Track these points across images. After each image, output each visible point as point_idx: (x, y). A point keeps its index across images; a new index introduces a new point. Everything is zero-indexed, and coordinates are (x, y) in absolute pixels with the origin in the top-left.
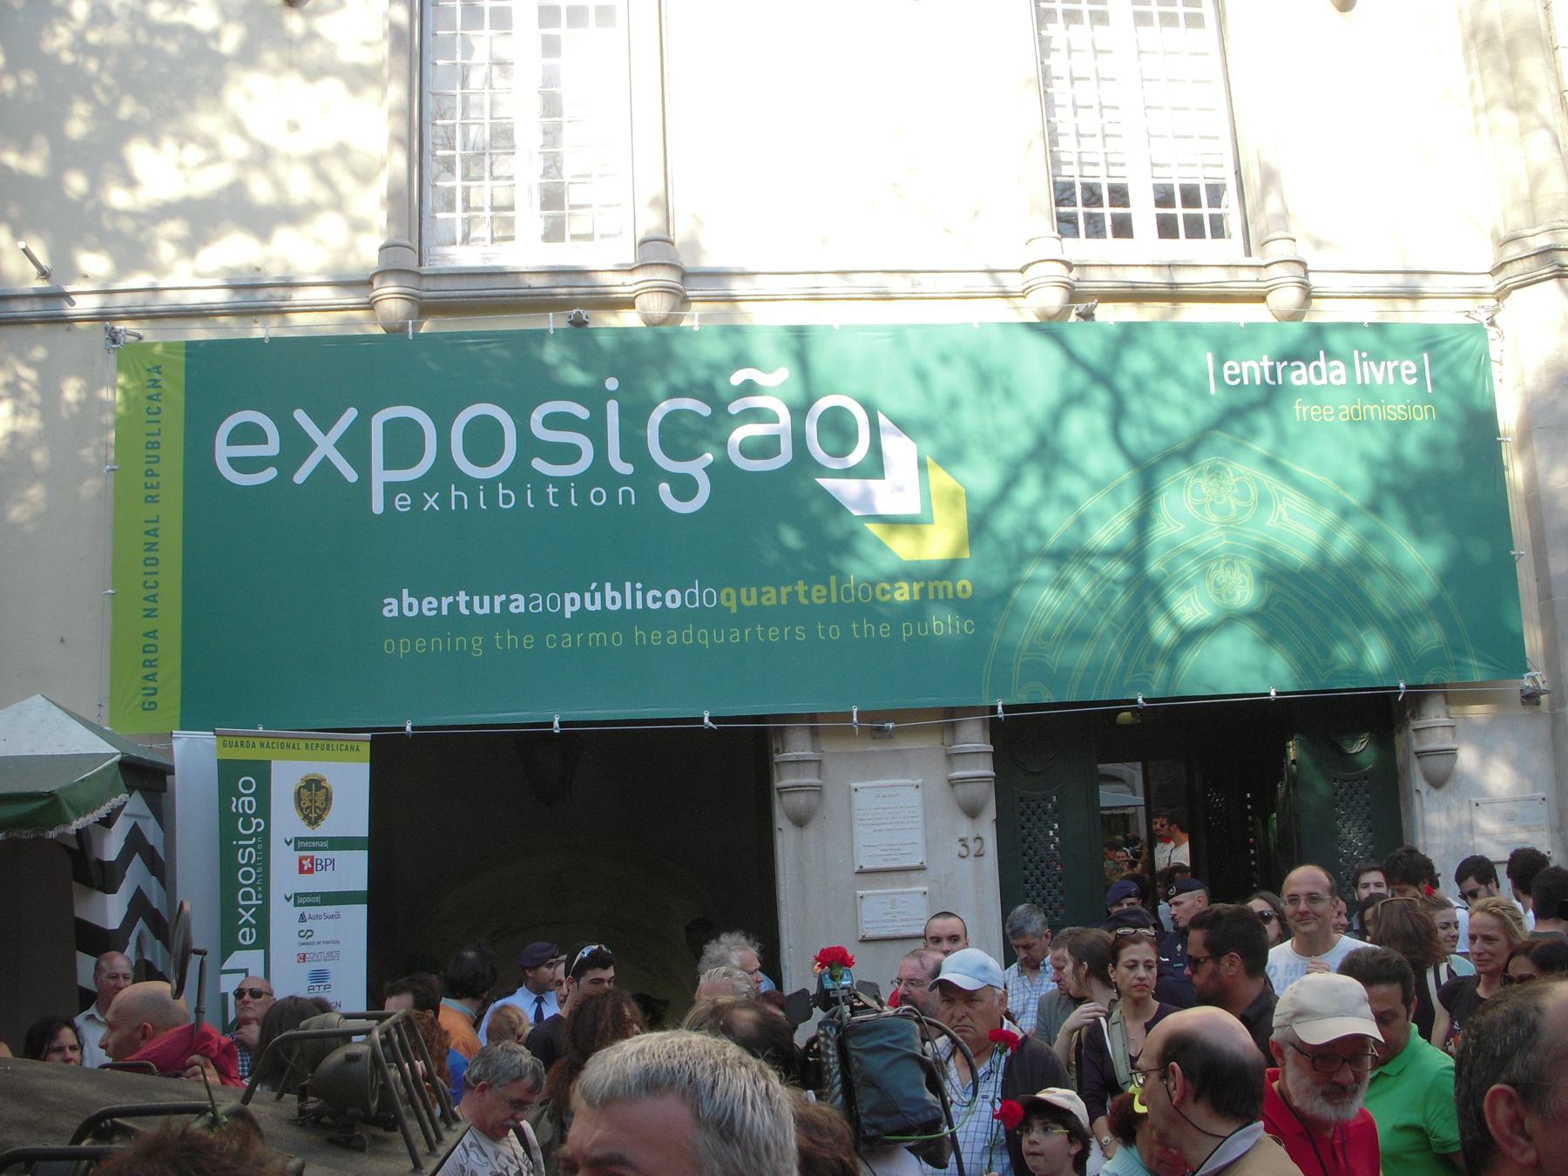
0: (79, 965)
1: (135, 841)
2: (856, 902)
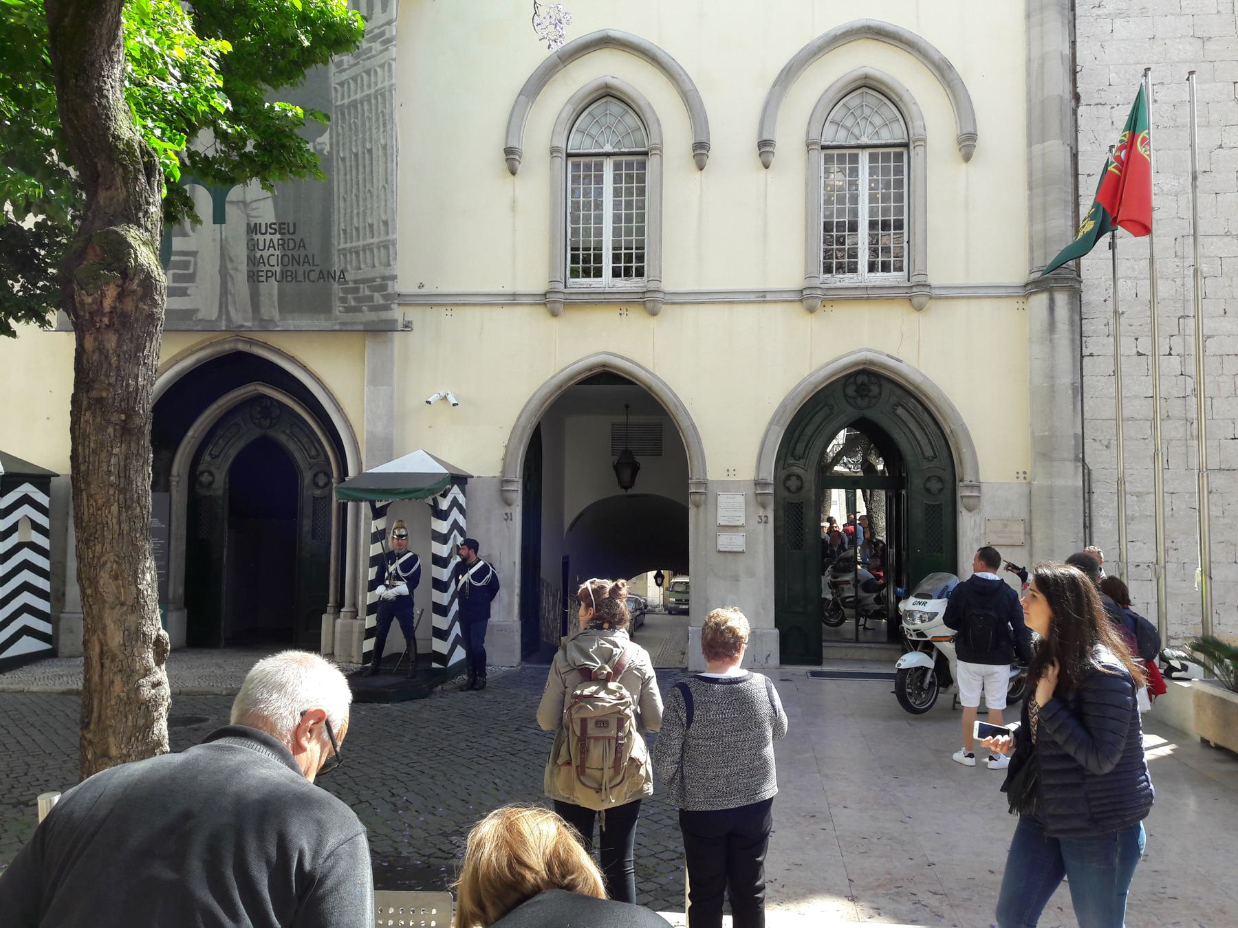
1: (455, 502)
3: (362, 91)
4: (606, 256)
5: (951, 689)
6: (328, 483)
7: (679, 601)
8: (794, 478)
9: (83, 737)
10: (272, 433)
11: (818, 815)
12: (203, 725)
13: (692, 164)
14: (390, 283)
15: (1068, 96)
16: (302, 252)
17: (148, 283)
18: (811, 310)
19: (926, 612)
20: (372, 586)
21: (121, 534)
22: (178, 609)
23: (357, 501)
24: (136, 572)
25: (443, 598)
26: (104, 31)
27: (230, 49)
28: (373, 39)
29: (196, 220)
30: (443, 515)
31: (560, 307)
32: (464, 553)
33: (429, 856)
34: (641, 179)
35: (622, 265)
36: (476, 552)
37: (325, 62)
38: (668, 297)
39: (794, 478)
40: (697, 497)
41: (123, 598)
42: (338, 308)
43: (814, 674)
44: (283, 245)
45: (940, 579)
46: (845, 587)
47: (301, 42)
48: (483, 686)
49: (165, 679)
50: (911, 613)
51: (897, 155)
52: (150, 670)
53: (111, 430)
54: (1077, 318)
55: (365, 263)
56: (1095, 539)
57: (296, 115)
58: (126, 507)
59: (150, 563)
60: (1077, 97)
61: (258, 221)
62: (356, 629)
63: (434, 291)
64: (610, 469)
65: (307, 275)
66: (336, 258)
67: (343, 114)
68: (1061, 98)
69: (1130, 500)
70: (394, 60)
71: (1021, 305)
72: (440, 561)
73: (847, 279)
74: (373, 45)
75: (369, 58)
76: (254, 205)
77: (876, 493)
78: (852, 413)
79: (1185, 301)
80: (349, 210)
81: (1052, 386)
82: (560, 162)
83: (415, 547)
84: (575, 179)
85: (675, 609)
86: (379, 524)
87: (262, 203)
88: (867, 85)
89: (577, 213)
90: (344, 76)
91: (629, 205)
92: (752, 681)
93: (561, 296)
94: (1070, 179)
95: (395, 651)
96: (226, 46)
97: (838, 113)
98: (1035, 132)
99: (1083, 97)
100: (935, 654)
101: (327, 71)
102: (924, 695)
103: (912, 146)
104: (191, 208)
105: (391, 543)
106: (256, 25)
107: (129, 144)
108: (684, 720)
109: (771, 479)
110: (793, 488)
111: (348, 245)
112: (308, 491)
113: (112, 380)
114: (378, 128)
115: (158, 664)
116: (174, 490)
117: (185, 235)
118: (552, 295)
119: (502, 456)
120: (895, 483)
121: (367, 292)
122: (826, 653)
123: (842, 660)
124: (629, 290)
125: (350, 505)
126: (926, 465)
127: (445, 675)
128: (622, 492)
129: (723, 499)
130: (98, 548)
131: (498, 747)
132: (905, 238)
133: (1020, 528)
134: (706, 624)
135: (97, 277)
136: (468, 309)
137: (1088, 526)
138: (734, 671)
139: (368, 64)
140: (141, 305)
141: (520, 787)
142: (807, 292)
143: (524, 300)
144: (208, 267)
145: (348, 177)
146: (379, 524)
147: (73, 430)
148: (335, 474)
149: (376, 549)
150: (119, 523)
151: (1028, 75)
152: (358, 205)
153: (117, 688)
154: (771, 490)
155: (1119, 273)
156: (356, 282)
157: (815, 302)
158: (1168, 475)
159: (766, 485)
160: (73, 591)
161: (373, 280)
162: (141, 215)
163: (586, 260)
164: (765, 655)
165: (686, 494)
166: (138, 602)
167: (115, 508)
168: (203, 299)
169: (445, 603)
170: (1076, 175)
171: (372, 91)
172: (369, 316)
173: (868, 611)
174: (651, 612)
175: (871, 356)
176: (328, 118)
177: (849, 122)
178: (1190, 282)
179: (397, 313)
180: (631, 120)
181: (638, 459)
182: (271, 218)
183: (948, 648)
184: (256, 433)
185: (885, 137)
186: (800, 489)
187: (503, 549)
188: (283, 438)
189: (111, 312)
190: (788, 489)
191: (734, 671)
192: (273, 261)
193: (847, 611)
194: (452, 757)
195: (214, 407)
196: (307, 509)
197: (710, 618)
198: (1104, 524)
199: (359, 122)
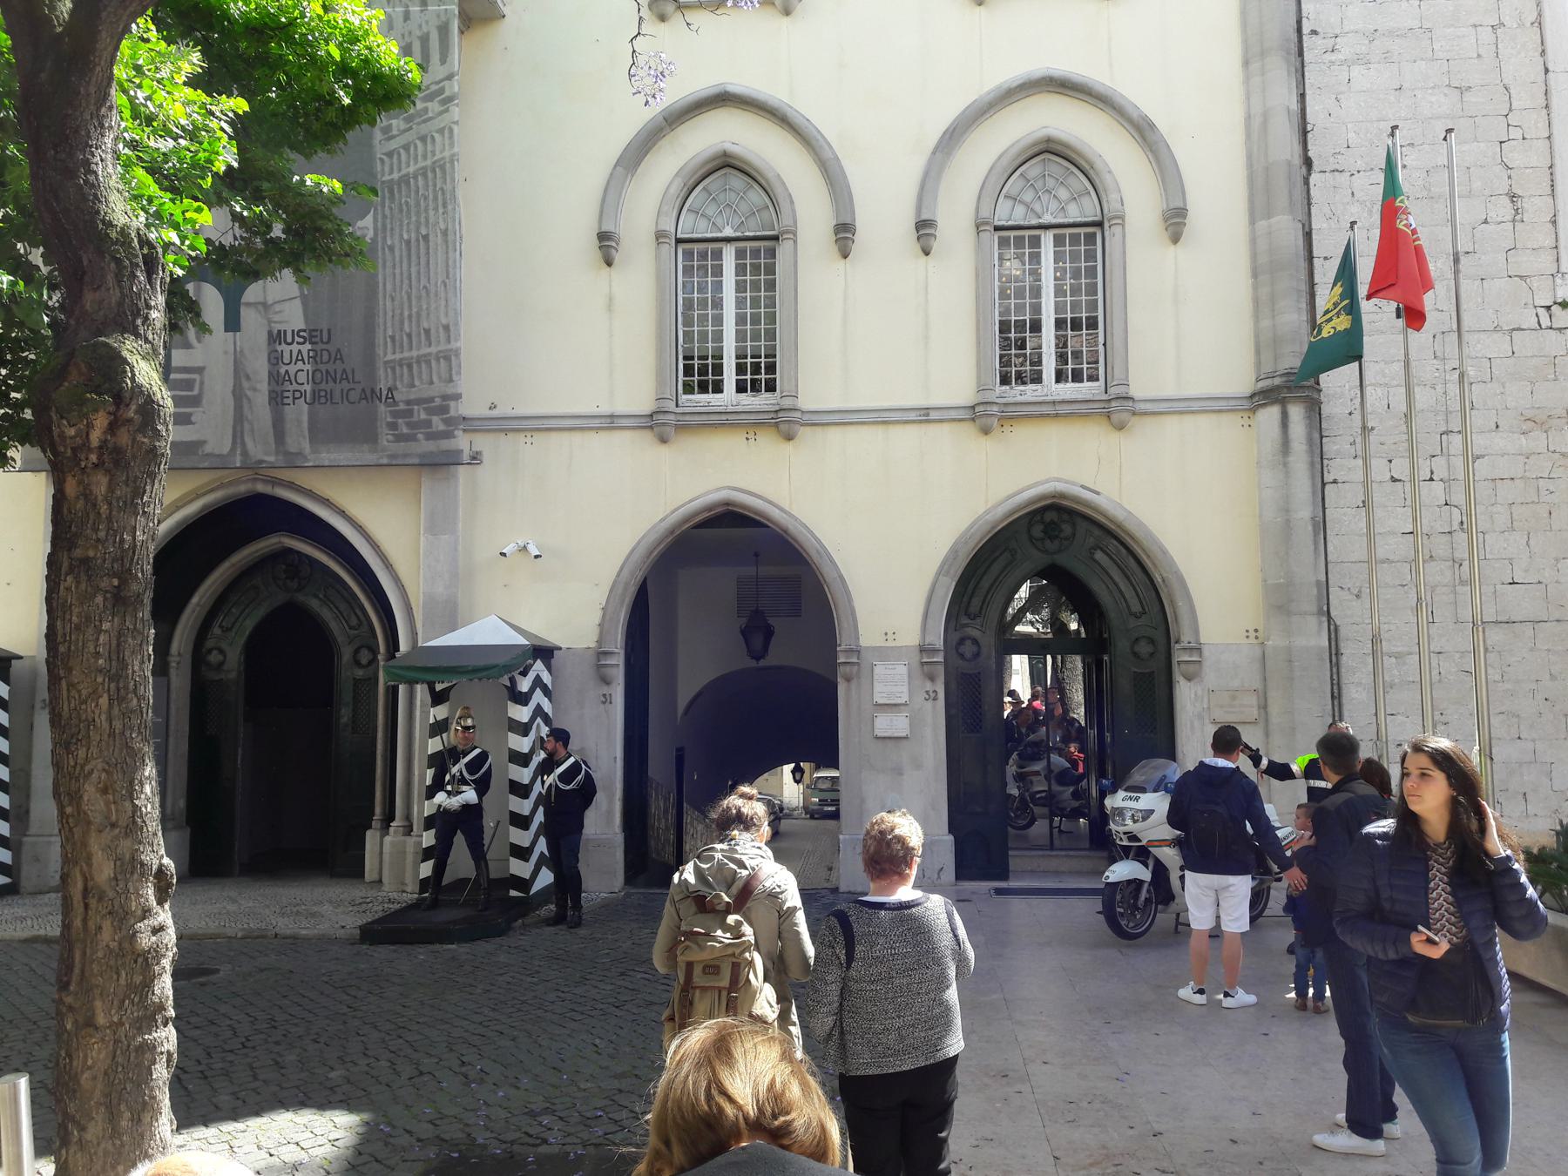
1: (538, 682)
3: (416, 162)
4: (728, 366)
5: (1173, 907)
6: (374, 661)
7: (823, 802)
8: (968, 643)
9: (60, 1001)
10: (300, 597)
11: (1011, 1074)
12: (213, 978)
13: (834, 250)
14: (452, 404)
15: (1297, 160)
16: (339, 366)
17: (149, 408)
18: (986, 431)
19: (1142, 810)
20: (431, 793)
21: (112, 734)
22: (176, 828)
23: (411, 683)
24: (131, 783)
25: (524, 806)
26: (92, 90)
27: (247, 108)
28: (430, 98)
29: (204, 329)
30: (523, 699)
31: (670, 431)
32: (549, 746)
33: (512, 1143)
34: (771, 270)
35: (749, 377)
36: (566, 744)
37: (373, 123)
38: (806, 417)
39: (968, 643)
40: (848, 668)
41: (114, 818)
42: (385, 438)
43: (999, 892)
44: (315, 358)
45: (1155, 768)
46: (1034, 778)
47: (339, 100)
48: (577, 924)
49: (170, 922)
50: (1120, 812)
51: (1088, 237)
52: (149, 910)
53: (99, 599)
54: (1317, 435)
55: (420, 378)
56: (1346, 714)
57: (333, 191)
58: (118, 698)
59: (150, 770)
60: (1308, 163)
61: (282, 327)
62: (410, 849)
63: (509, 412)
64: (736, 637)
65: (345, 395)
66: (381, 372)
67: (391, 192)
68: (1289, 163)
69: (1389, 662)
70: (456, 123)
71: (1246, 421)
72: (522, 759)
73: (1030, 392)
74: (429, 104)
75: (424, 121)
76: (277, 308)
77: (1069, 658)
78: (1039, 559)
79: (1447, 413)
80: (398, 312)
81: (1288, 521)
82: (668, 249)
83: (484, 741)
84: (688, 271)
85: (817, 812)
86: (440, 712)
87: (287, 304)
88: (1051, 150)
89: (690, 310)
90: (393, 145)
91: (755, 302)
92: (928, 904)
93: (672, 417)
94: (1303, 264)
95: (461, 876)
96: (241, 105)
97: (1014, 185)
98: (1258, 207)
99: (1316, 163)
100: (1151, 863)
101: (371, 137)
102: (1141, 915)
103: (1106, 225)
104: (198, 315)
105: (452, 737)
106: (283, 78)
107: (124, 232)
108: (843, 957)
109: (940, 644)
110: (968, 655)
111: (398, 356)
112: (347, 672)
113: (102, 534)
114: (436, 209)
115: (160, 903)
116: (173, 672)
117: (187, 345)
118: (661, 416)
119: (597, 620)
120: (1095, 647)
121: (423, 416)
122: (1016, 861)
123: (1033, 873)
124: (758, 408)
125: (401, 687)
126: (1132, 623)
127: (526, 906)
128: (753, 663)
129: (879, 670)
130: (82, 753)
131: (598, 997)
132: (1101, 339)
133: (1253, 700)
134: (868, 833)
135: (83, 402)
136: (554, 436)
137: (1337, 696)
138: (905, 892)
139: (424, 129)
140: (140, 438)
141: (628, 1049)
142: (981, 408)
143: (625, 422)
144: (218, 387)
145: (397, 271)
146: (440, 712)
147: (49, 600)
148: (382, 648)
149: (435, 745)
150: (110, 720)
151: (1248, 136)
152: (410, 307)
153: (107, 936)
154: (940, 658)
155: (1367, 381)
156: (408, 402)
157: (989, 421)
158: (1434, 629)
159: (934, 651)
160: (44, 808)
161: (432, 400)
162: (139, 322)
163: (703, 371)
164: (938, 867)
165: (833, 665)
166: (134, 822)
167: (104, 701)
168: (212, 427)
169: (526, 812)
170: (1310, 258)
171: (429, 162)
172: (425, 446)
173: (1063, 809)
174: (788, 816)
175: (1061, 487)
176: (374, 191)
177: (1028, 196)
178: (1454, 389)
179: (462, 442)
180: (756, 197)
181: (771, 621)
182: (299, 324)
183: (1170, 857)
184: (280, 598)
185: (1074, 214)
186: (977, 655)
187: (601, 743)
188: (314, 604)
189: (100, 448)
190: (962, 656)
191: (905, 892)
192: (302, 377)
193: (1038, 810)
194: (539, 1012)
195: (226, 565)
196: (347, 697)
197: (873, 825)
198: (1356, 694)
199: (412, 202)
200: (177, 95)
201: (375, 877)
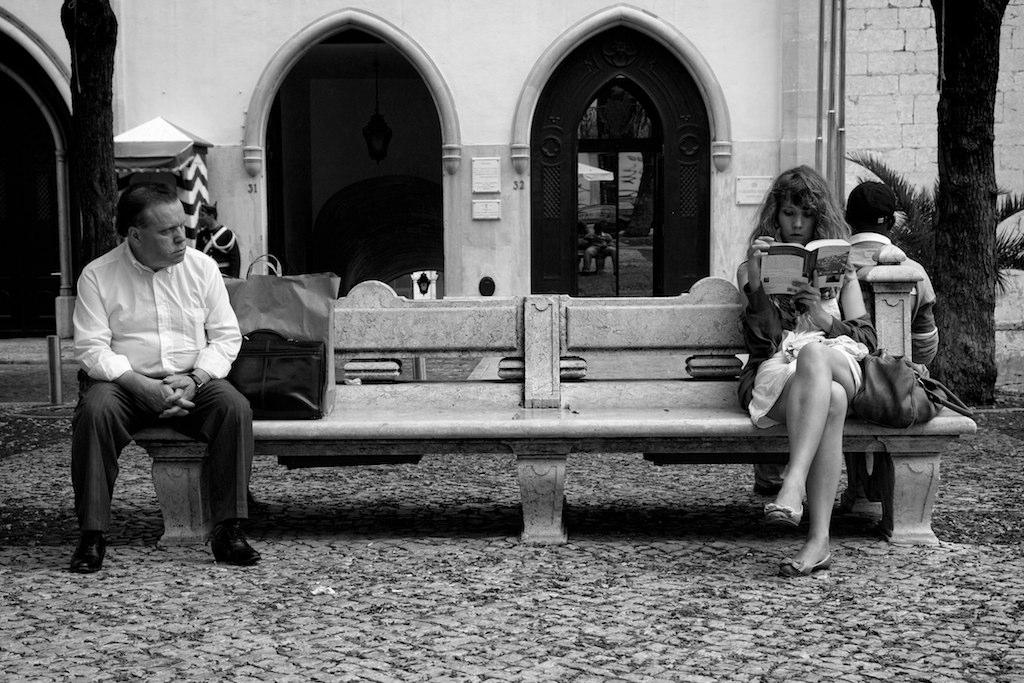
0: (846, 165)
1: (198, 173)
2: (472, 204)
129: (479, 163)
154: (527, 154)
200: (448, 647)
201: (66, 334)
